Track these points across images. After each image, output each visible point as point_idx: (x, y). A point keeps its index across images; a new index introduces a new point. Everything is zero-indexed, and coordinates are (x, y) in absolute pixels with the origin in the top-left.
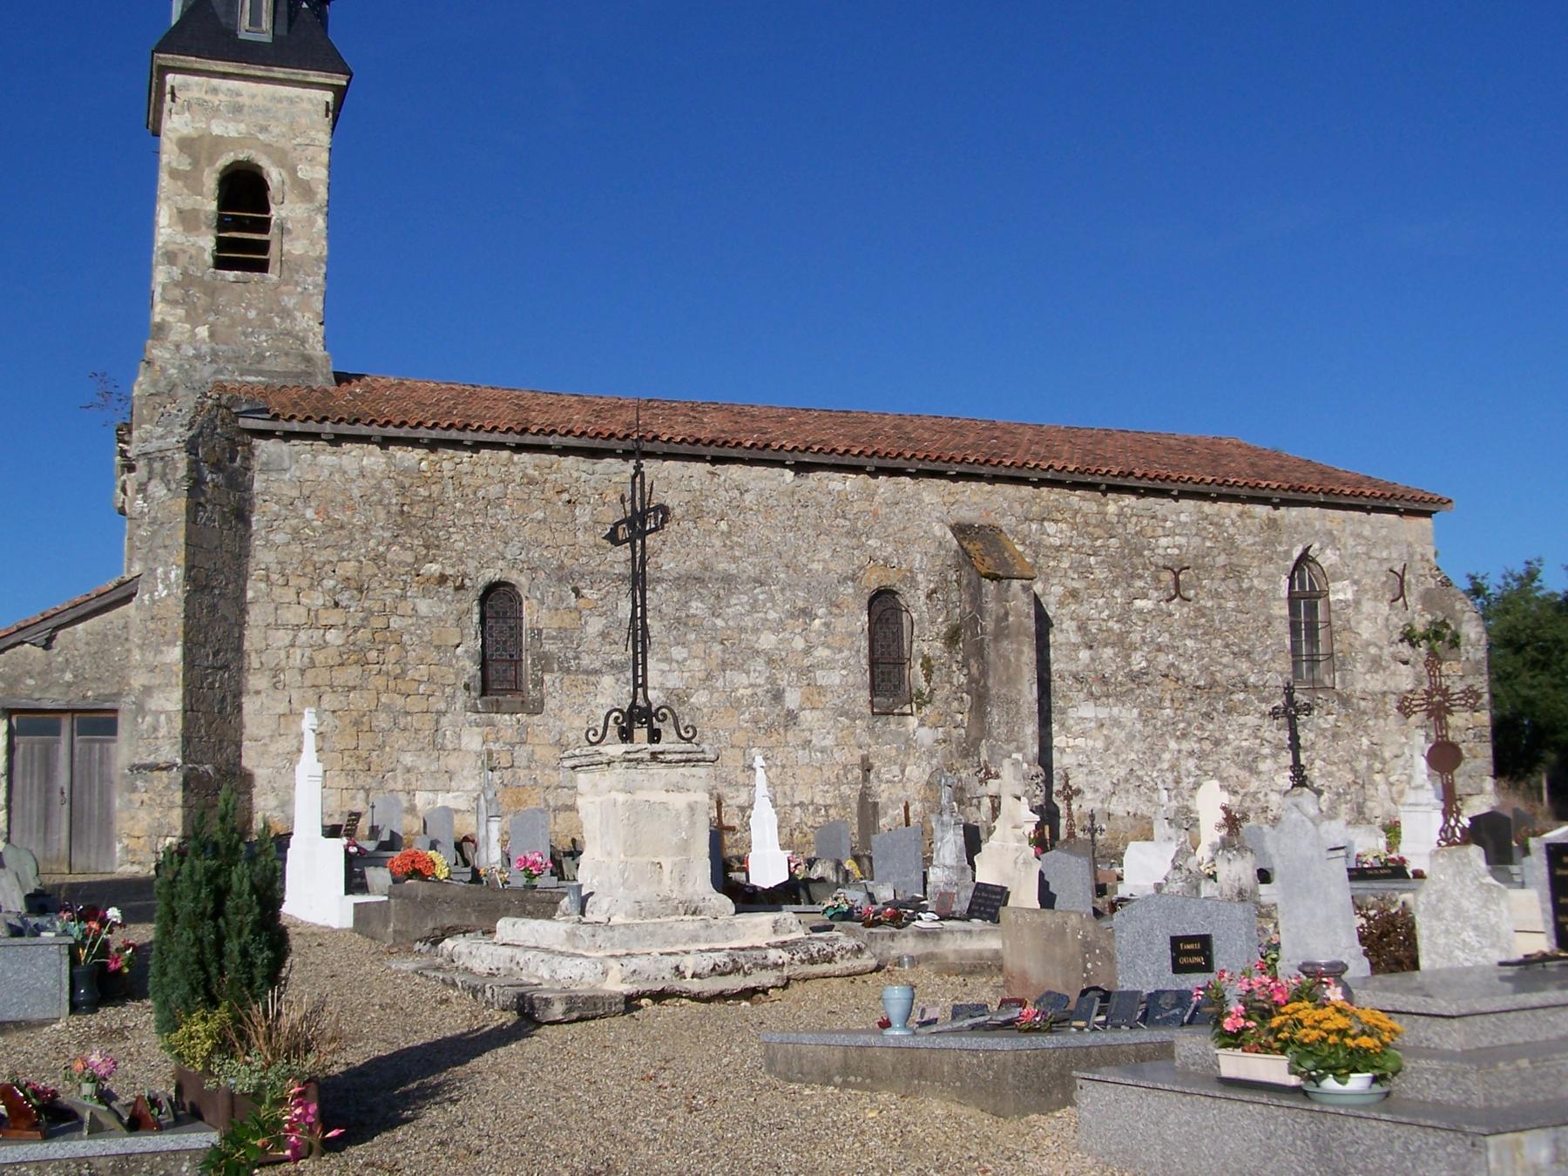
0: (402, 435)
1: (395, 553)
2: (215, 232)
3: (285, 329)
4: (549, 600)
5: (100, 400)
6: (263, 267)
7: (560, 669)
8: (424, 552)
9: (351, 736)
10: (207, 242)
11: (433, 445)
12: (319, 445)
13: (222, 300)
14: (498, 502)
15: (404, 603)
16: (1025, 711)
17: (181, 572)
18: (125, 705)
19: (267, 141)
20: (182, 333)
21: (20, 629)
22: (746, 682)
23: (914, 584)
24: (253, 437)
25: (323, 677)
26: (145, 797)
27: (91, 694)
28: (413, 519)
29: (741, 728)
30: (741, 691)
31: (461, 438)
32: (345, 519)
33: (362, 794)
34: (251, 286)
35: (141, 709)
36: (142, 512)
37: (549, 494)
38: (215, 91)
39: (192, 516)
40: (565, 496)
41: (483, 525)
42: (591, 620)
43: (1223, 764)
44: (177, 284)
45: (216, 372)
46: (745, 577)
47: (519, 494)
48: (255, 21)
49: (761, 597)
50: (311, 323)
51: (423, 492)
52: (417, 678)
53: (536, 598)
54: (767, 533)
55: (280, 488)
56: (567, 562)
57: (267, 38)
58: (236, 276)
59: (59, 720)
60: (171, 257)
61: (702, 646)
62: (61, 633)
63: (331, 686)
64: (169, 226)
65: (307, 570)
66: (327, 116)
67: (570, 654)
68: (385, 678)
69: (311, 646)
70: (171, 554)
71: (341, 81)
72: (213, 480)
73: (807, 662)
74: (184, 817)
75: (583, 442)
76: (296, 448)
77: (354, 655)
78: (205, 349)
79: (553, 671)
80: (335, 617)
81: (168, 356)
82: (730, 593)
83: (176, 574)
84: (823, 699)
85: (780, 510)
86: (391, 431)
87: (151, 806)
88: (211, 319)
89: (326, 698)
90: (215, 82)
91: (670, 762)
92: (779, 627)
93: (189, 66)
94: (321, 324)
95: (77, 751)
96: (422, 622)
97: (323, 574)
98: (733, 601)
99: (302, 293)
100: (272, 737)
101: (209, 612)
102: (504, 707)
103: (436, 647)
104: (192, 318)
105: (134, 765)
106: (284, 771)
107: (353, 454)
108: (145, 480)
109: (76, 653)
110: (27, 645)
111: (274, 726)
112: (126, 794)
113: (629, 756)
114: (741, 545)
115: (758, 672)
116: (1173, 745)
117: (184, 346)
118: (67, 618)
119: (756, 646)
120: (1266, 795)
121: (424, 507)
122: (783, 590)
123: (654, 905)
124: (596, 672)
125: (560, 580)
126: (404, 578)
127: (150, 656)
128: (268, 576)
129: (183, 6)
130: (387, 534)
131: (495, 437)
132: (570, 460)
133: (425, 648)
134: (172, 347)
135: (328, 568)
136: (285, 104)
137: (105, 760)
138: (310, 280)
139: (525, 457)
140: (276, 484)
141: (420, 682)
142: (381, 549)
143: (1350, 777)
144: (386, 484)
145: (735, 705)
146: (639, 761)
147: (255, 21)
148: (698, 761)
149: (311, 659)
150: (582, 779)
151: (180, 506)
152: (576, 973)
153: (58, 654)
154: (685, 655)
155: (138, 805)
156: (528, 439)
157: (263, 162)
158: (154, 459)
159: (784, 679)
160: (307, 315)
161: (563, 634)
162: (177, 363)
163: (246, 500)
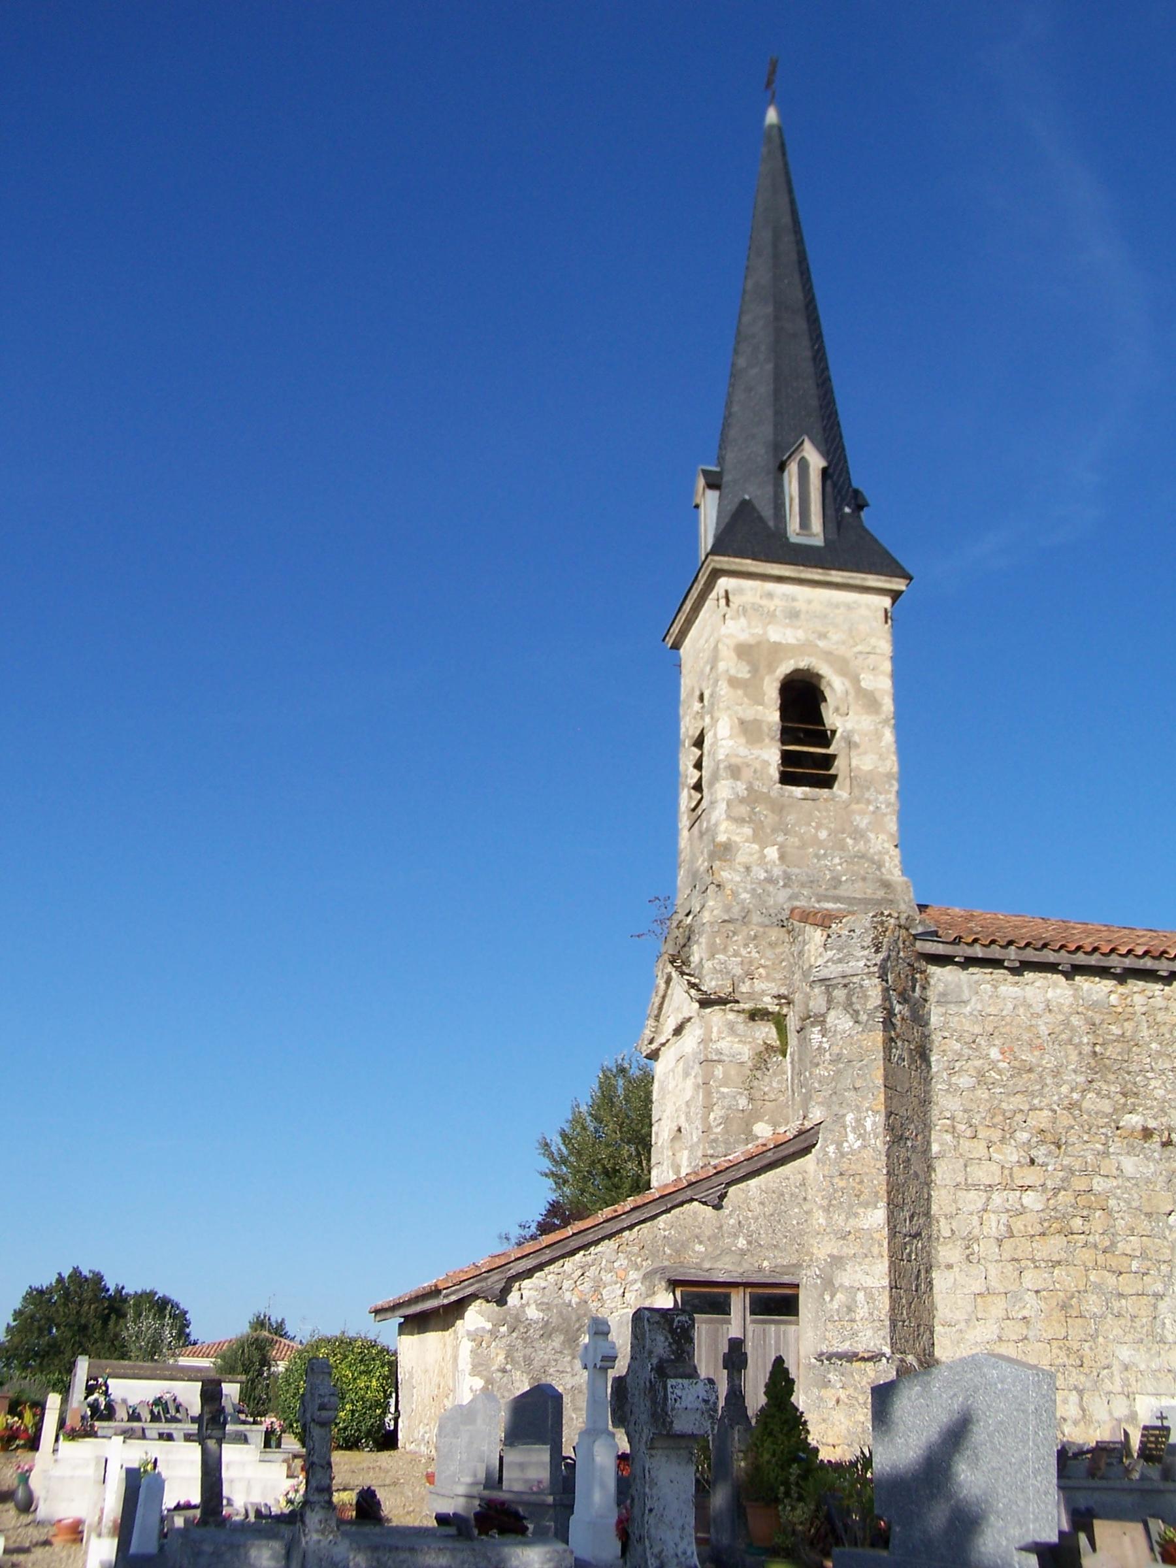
0: (1093, 963)
2: (779, 744)
3: (859, 851)
6: (828, 782)
8: (1123, 1101)
10: (771, 755)
11: (1122, 977)
12: (1000, 973)
13: (791, 818)
15: (1107, 1161)
17: (880, 1119)
20: (751, 854)
21: (691, 1184)
25: (1024, 1248)
26: (842, 1394)
28: (1107, 1061)
31: (1155, 968)
34: (821, 804)
35: (829, 1284)
36: (819, 1048)
38: (770, 595)
44: (742, 801)
45: (790, 898)
50: (886, 845)
51: (1116, 1030)
52: (1129, 1252)
55: (960, 1022)
57: (818, 541)
58: (803, 793)
59: (727, 1297)
60: (735, 772)
62: (732, 1190)
63: (1033, 1260)
64: (731, 737)
65: (996, 1120)
66: (886, 622)
68: (1093, 1251)
69: (1008, 1211)
70: (864, 1098)
71: (899, 584)
76: (975, 977)
78: (777, 872)
80: (1031, 1176)
81: (738, 879)
83: (874, 1121)
86: (1081, 959)
88: (780, 839)
90: (770, 586)
94: (896, 846)
96: (1128, 1184)
99: (874, 812)
100: (967, 1321)
103: (1146, 1214)
104: (759, 837)
105: (822, 1354)
107: (1037, 984)
109: (750, 1214)
110: (696, 1203)
111: (970, 1309)
117: (755, 869)
121: (1119, 1047)
126: (1103, 1130)
127: (839, 1219)
128: (954, 1127)
134: (742, 870)
135: (1019, 1117)
136: (842, 610)
138: (882, 798)
141: (1133, 1257)
142: (1075, 1096)
144: (1075, 1020)
151: (874, 1041)
157: (824, 669)
158: (835, 986)
162: (749, 887)
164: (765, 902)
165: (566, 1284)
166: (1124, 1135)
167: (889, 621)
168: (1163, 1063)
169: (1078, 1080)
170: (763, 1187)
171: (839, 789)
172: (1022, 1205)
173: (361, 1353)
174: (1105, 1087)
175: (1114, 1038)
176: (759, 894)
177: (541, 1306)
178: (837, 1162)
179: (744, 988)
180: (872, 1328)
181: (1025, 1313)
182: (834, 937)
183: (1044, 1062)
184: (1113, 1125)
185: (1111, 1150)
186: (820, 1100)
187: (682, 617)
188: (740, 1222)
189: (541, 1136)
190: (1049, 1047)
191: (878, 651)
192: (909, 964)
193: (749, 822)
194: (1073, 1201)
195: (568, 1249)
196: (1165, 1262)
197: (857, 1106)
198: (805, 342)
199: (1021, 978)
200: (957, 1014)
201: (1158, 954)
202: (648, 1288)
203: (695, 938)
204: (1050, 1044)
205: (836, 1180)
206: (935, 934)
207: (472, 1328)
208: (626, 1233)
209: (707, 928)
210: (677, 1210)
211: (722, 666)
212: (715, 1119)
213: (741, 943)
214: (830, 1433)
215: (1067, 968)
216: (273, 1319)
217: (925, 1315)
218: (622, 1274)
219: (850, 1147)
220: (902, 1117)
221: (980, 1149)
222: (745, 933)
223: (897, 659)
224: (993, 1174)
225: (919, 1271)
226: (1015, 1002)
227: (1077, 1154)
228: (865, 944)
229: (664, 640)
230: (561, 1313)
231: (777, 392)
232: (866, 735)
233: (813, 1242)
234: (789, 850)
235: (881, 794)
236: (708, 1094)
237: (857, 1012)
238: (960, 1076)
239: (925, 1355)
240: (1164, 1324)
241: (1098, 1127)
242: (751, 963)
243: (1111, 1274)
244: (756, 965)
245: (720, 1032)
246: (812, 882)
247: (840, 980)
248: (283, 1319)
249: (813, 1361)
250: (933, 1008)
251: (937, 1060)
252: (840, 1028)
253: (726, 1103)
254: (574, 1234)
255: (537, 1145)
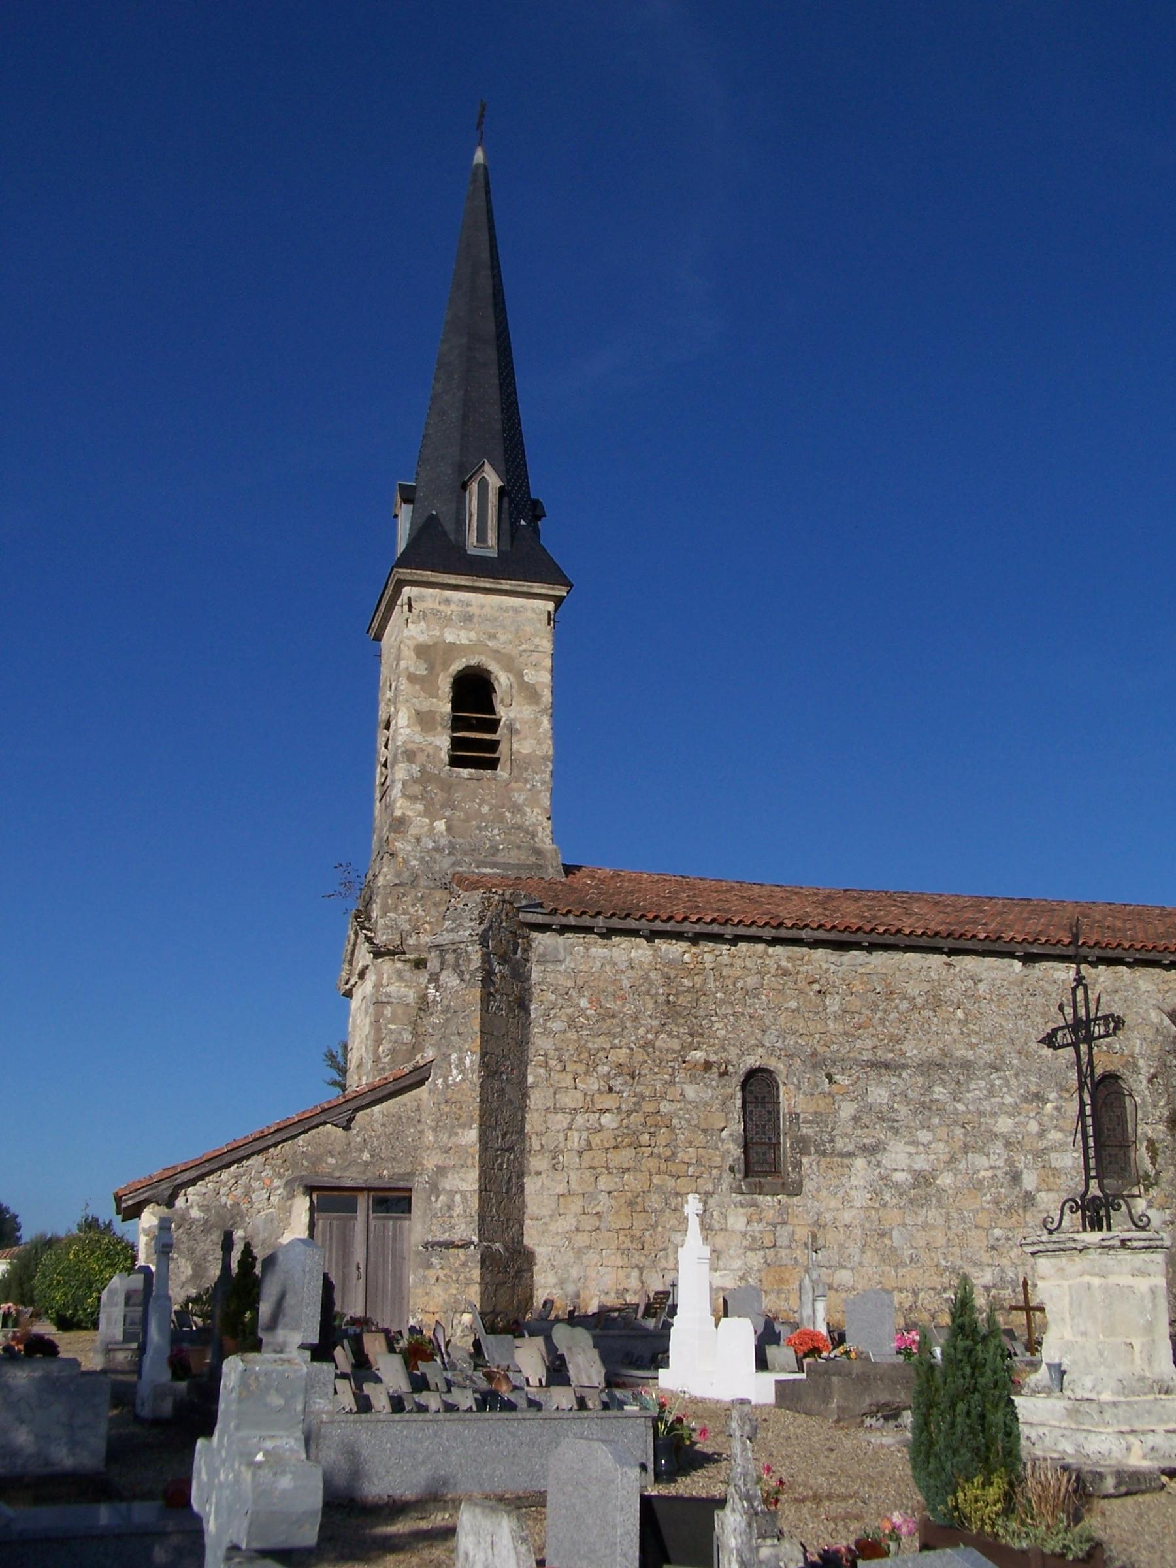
0: (669, 929)
1: (663, 1040)
3: (516, 823)
4: (805, 1086)
5: (342, 889)
6: (492, 764)
7: (817, 1151)
8: (690, 1040)
9: (626, 1216)
10: (443, 741)
11: (696, 939)
12: (591, 938)
13: (458, 796)
14: (755, 993)
15: (672, 1088)
17: (477, 1058)
18: (419, 1185)
19: (495, 648)
20: (422, 827)
21: (324, 1111)
22: (987, 1165)
23: (1136, 1069)
24: (531, 929)
25: (599, 1158)
26: (441, 1274)
27: (386, 1173)
29: (983, 1209)
30: (982, 1173)
31: (722, 932)
32: (616, 1008)
33: (635, 1273)
34: (484, 783)
35: (434, 1189)
37: (802, 984)
38: (448, 602)
39: (485, 1006)
40: (816, 987)
41: (743, 1014)
42: (843, 1105)
44: (415, 781)
45: (454, 864)
46: (981, 1063)
47: (775, 985)
48: (482, 537)
49: (997, 1082)
50: (540, 818)
52: (687, 1160)
53: (793, 1083)
54: (1000, 1020)
55: (556, 978)
56: (820, 1049)
57: (493, 553)
59: (356, 1198)
60: (410, 756)
61: (945, 1129)
62: (359, 1114)
63: (607, 1168)
64: (408, 726)
65: (582, 1057)
66: (549, 624)
67: (826, 1138)
68: (656, 1160)
69: (588, 1129)
70: (465, 1041)
71: (561, 591)
72: (500, 971)
73: (1041, 1145)
74: (481, 1293)
75: (833, 936)
76: (571, 941)
77: (628, 1139)
78: (443, 842)
79: (810, 1154)
80: (609, 1101)
81: (409, 848)
82: (969, 1078)
83: (471, 1060)
84: (1058, 1181)
85: (1010, 998)
86: (658, 925)
87: (447, 1282)
89: (603, 1180)
90: (448, 593)
91: (1135, 1248)
92: (1015, 1111)
93: (425, 579)
94: (549, 819)
95: (372, 1228)
97: (597, 1060)
98: (972, 1086)
99: (530, 790)
100: (551, 1216)
101: (498, 1097)
102: (766, 1189)
103: (703, 1130)
105: (427, 1243)
106: (563, 1249)
108: (438, 970)
109: (373, 1134)
111: (554, 1206)
112: (421, 1271)
113: (1104, 1243)
114: (976, 1033)
115: (997, 1155)
117: (424, 840)
118: (366, 1102)
119: (995, 1129)
122: (1017, 1075)
123: (1134, 1383)
124: (850, 1155)
125: (814, 1066)
126: (670, 1064)
127: (444, 1138)
128: (547, 1062)
129: (412, 524)
130: (655, 1023)
131: (753, 931)
132: (820, 953)
133: (694, 1132)
134: (413, 840)
135: (602, 1054)
137: (398, 1236)
138: (537, 777)
139: (779, 949)
140: (553, 975)
142: (650, 1036)
144: (653, 975)
145: (977, 1186)
146: (1110, 1247)
147: (482, 537)
148: (1157, 1247)
149: (589, 1143)
150: (1043, 1263)
152: (1104, 1448)
153: (357, 1135)
154: (930, 1138)
155: (433, 1281)
156: (783, 933)
157: (493, 666)
158: (447, 951)
159: (1021, 1161)
160: (536, 810)
161: (818, 1118)
163: (526, 990)
164: (432, 868)
165: (223, 1190)
166: (689, 1067)
167: (552, 622)
168: (726, 1009)
169: (653, 1024)
170: (385, 1112)
171: (502, 770)
172: (600, 1124)
173: (107, 1249)
174: (675, 1029)
175: (685, 989)
176: (427, 862)
177: (202, 1208)
178: (444, 1092)
179: (411, 941)
180: (466, 1222)
181: (598, 1209)
182: (452, 909)
183: (625, 1009)
184: (680, 1059)
185: (677, 1079)
186: (433, 1042)
187: (380, 614)
188: (365, 1140)
189: (326, 1050)
190: (630, 999)
191: (540, 649)
192: (511, 932)
193: (421, 799)
194: (643, 1121)
195: (223, 1163)
196: (716, 1167)
197: (460, 1047)
198: (494, 370)
199: (609, 941)
200: (554, 971)
201: (723, 921)
202: (289, 1193)
203: (374, 898)
204: (631, 995)
205: (442, 1106)
206: (540, 905)
207: (147, 1226)
208: (272, 1150)
209: (381, 891)
210: (314, 1131)
211: (403, 664)
212: (383, 1051)
213: (409, 903)
214: (431, 1303)
215: (647, 933)
216: (101, 1221)
217: (515, 1211)
218: (268, 1182)
219: (454, 1080)
220: (497, 1056)
221: (568, 1080)
222: (413, 895)
223: (556, 655)
224: (577, 1100)
225: (510, 1178)
226: (603, 961)
227: (647, 1083)
228: (473, 917)
229: (368, 632)
230: (218, 1213)
231: (465, 417)
232: (526, 723)
233: (425, 1155)
234: (455, 822)
235: (537, 773)
236: (378, 1030)
237: (462, 972)
238: (553, 1022)
239: (513, 1243)
240: (712, 1215)
241: (668, 1062)
242: (417, 920)
243: (670, 1178)
244: (422, 922)
245: (389, 978)
246: (474, 850)
247: (450, 946)
248: (111, 1221)
249: (421, 1248)
250: (533, 966)
251: (535, 1009)
252: (449, 984)
253: (393, 1037)
254: (228, 1151)
255: (325, 1058)
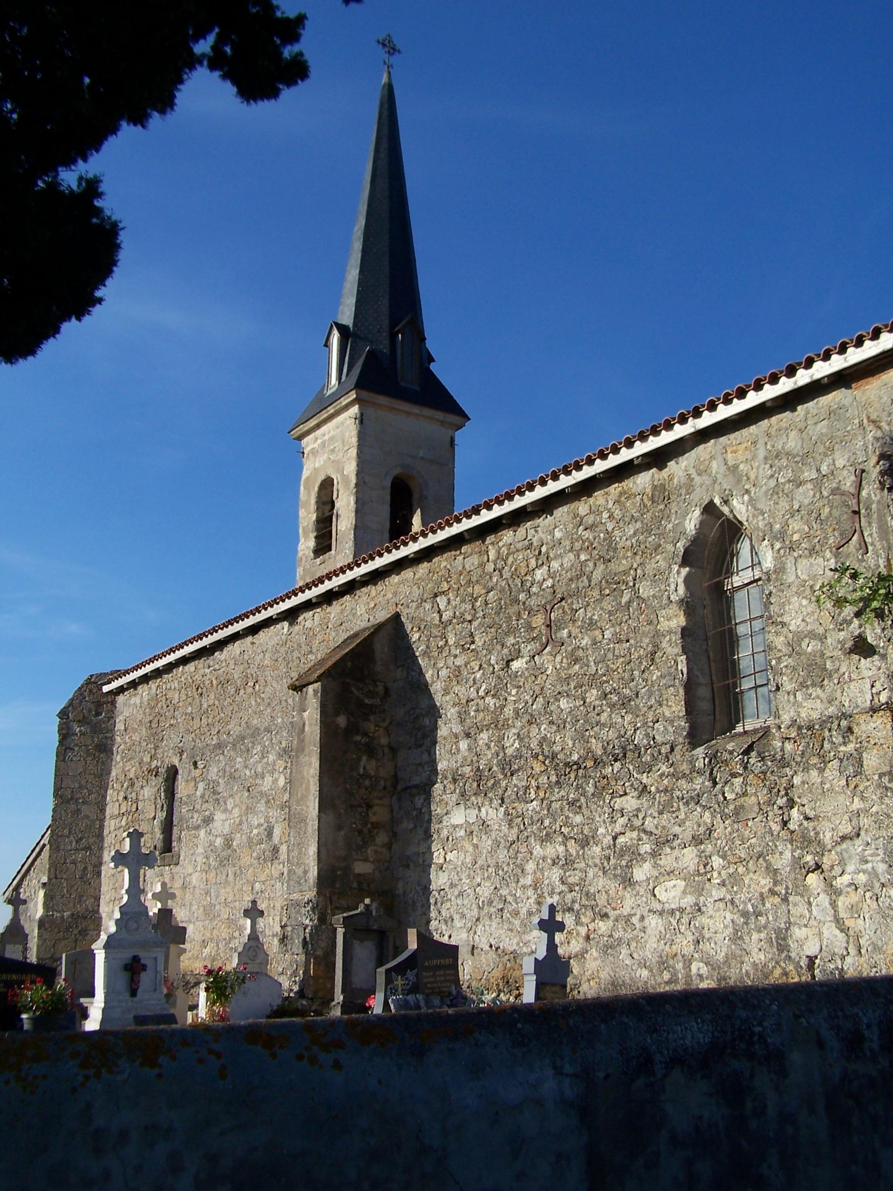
16: (310, 829)
43: (591, 874)
72: (80, 731)
116: (538, 851)
120: (642, 918)
143: (766, 882)
